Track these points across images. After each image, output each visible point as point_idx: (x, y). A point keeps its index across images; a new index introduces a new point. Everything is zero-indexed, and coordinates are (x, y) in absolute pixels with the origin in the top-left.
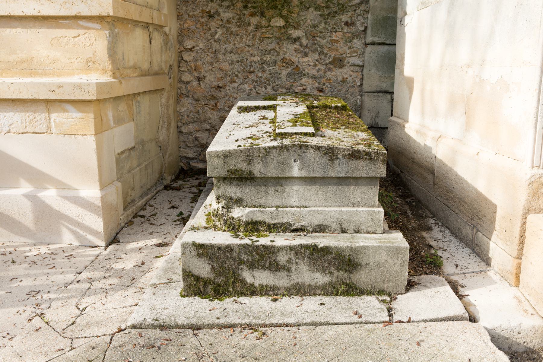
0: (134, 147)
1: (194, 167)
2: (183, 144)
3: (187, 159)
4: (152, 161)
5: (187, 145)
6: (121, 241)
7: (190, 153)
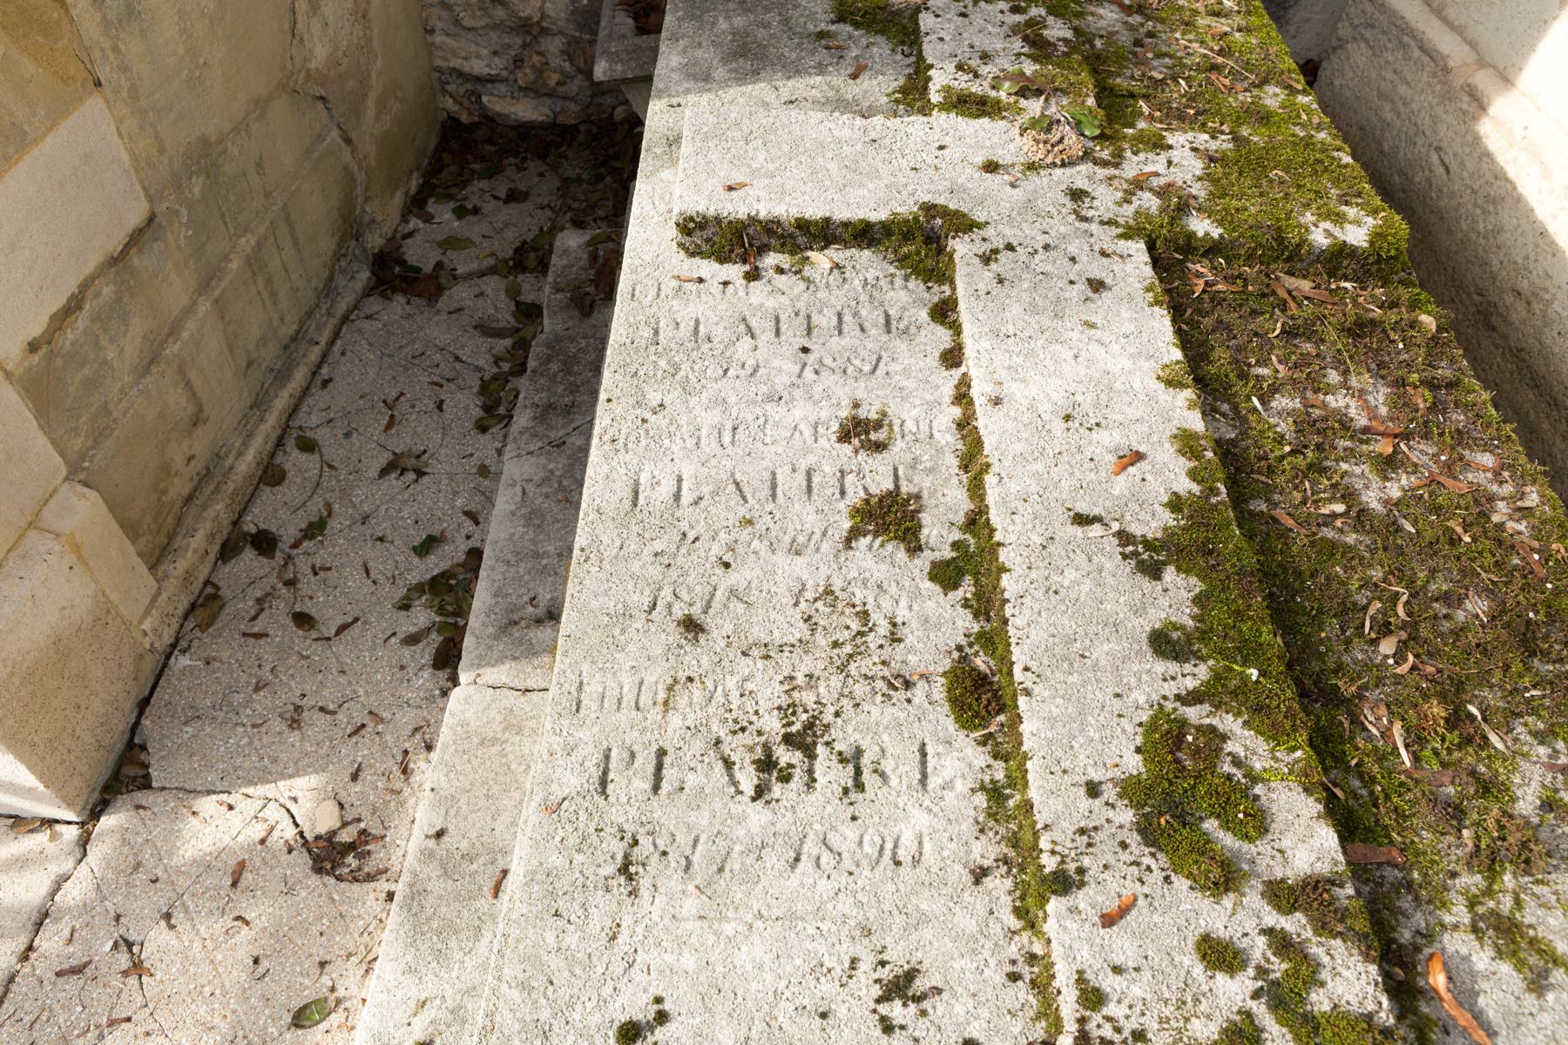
0: (151, 219)
1: (498, 114)
2: (444, 14)
3: (468, 81)
4: (285, 208)
5: (457, 22)
6: (157, 780)
7: (478, 56)
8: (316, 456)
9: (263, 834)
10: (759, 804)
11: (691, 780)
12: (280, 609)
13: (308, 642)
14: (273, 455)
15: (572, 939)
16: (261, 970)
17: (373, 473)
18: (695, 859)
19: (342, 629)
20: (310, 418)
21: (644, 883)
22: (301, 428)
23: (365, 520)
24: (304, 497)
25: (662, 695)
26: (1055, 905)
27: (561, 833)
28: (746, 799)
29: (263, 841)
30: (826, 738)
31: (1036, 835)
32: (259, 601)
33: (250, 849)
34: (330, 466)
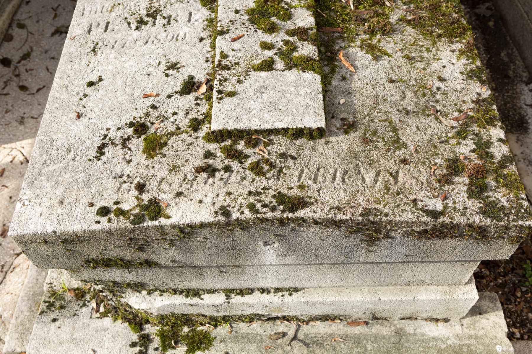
8: (25, 30)
9: (11, 159)
10: (137, 31)
11: (116, 27)
12: (14, 85)
13: (25, 95)
14: (7, 30)
15: (76, 66)
16: (12, 200)
17: (49, 34)
18: (115, 46)
19: (39, 90)
20: (22, 16)
21: (99, 52)
22: (18, 20)
23: (46, 52)
24: (21, 45)
25: (110, 9)
26: (219, 38)
27: (75, 44)
28: (133, 30)
29: (11, 162)
30: (160, 13)
31: (217, 23)
32: (5, 82)
33: (7, 164)
34: (31, 33)
